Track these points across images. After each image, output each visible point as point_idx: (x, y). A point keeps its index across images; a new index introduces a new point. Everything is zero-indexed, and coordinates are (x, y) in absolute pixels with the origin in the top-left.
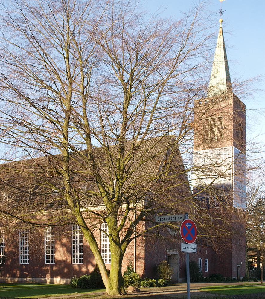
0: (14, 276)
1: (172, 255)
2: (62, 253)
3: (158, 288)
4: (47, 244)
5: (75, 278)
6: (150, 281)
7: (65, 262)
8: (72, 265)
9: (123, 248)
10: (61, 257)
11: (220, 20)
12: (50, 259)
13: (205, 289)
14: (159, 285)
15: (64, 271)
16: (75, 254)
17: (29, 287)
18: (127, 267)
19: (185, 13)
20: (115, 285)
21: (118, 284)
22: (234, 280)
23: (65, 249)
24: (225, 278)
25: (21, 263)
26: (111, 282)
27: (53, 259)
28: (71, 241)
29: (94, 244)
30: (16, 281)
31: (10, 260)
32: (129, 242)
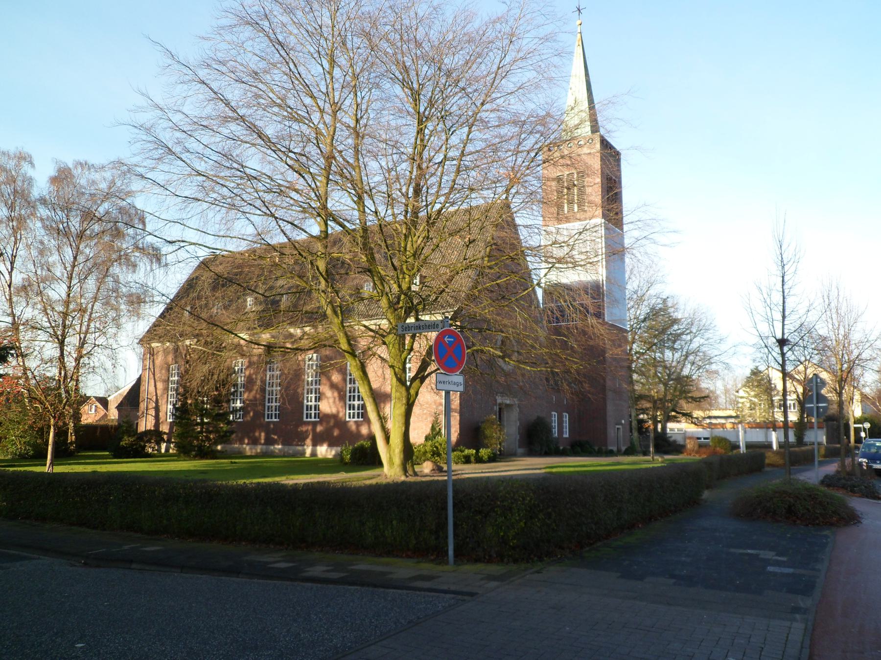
0: (255, 442)
1: (507, 406)
2: (331, 400)
3: (478, 466)
4: (308, 384)
5: (346, 445)
6: (467, 452)
7: (335, 417)
8: (346, 422)
9: (412, 392)
10: (330, 407)
11: (578, 22)
12: (313, 412)
13: (552, 467)
14: (479, 460)
15: (333, 434)
16: (352, 402)
17: (272, 462)
18: (431, 425)
19: (504, 3)
20: (398, 459)
21: (402, 456)
22: (610, 453)
23: (336, 394)
24: (596, 448)
25: (268, 418)
26: (392, 451)
27: (317, 412)
28: (345, 380)
29: (365, 383)
30: (259, 451)
31: (251, 414)
32: (423, 380)
